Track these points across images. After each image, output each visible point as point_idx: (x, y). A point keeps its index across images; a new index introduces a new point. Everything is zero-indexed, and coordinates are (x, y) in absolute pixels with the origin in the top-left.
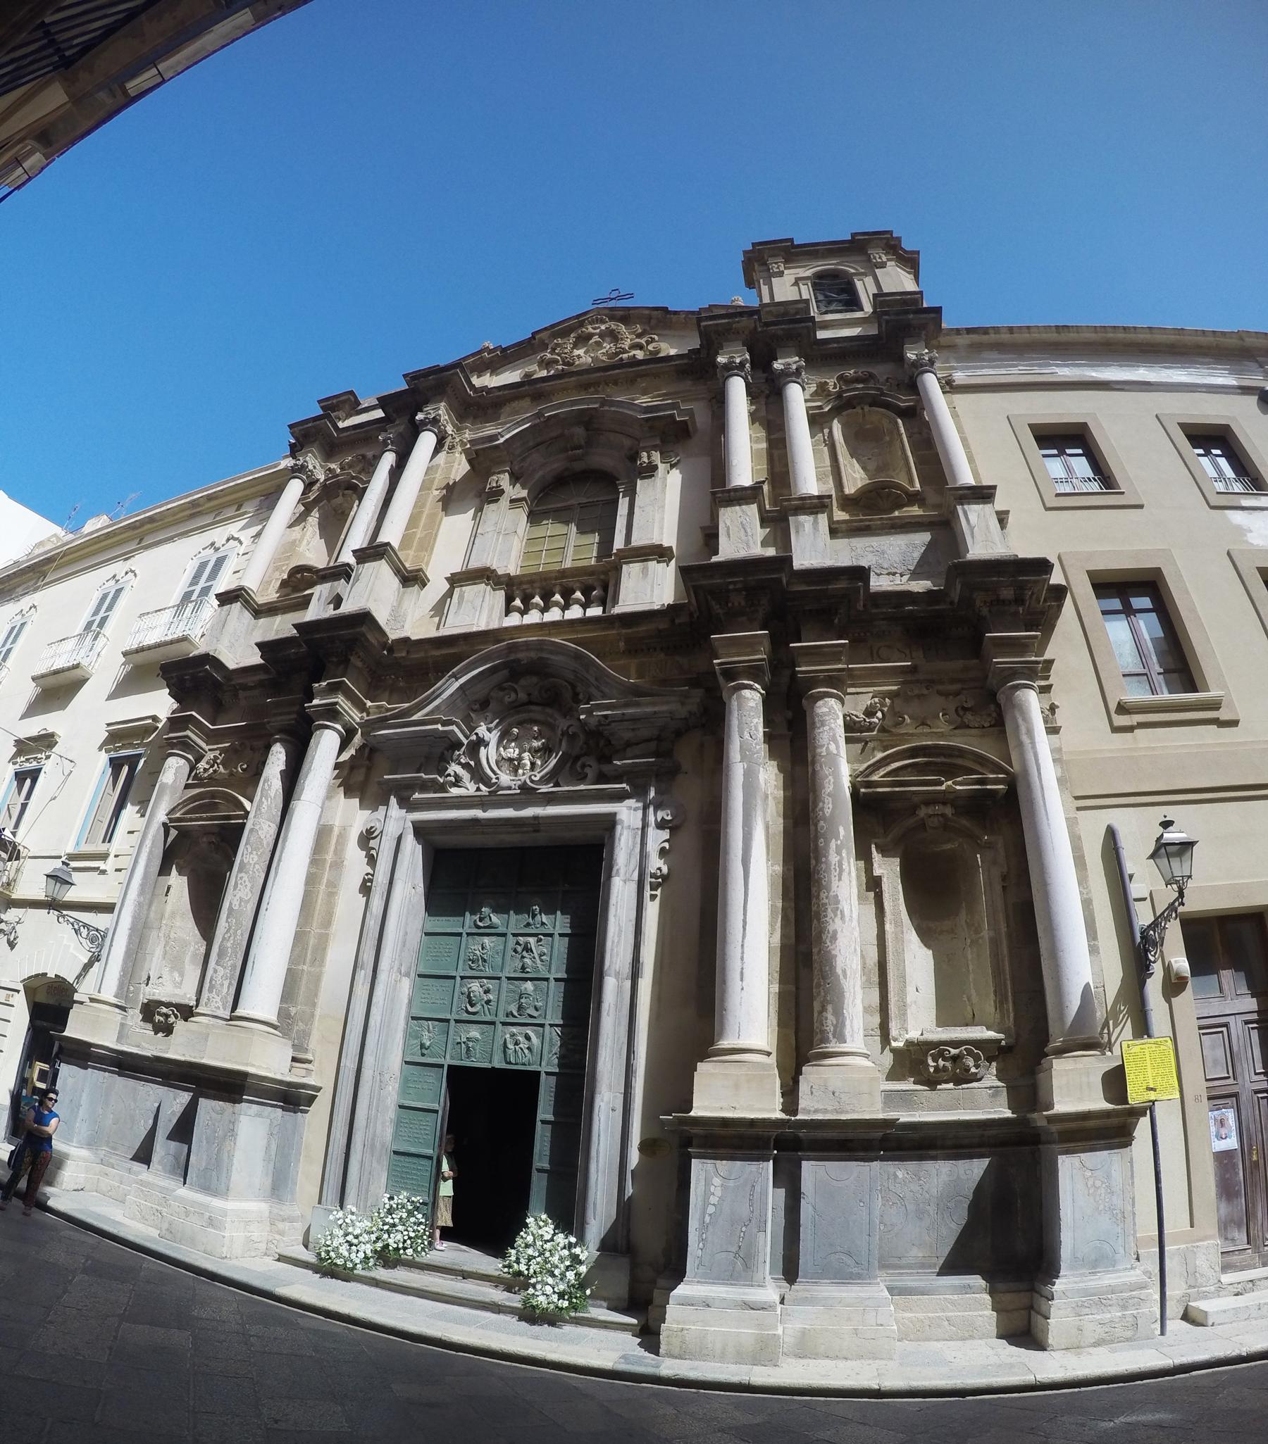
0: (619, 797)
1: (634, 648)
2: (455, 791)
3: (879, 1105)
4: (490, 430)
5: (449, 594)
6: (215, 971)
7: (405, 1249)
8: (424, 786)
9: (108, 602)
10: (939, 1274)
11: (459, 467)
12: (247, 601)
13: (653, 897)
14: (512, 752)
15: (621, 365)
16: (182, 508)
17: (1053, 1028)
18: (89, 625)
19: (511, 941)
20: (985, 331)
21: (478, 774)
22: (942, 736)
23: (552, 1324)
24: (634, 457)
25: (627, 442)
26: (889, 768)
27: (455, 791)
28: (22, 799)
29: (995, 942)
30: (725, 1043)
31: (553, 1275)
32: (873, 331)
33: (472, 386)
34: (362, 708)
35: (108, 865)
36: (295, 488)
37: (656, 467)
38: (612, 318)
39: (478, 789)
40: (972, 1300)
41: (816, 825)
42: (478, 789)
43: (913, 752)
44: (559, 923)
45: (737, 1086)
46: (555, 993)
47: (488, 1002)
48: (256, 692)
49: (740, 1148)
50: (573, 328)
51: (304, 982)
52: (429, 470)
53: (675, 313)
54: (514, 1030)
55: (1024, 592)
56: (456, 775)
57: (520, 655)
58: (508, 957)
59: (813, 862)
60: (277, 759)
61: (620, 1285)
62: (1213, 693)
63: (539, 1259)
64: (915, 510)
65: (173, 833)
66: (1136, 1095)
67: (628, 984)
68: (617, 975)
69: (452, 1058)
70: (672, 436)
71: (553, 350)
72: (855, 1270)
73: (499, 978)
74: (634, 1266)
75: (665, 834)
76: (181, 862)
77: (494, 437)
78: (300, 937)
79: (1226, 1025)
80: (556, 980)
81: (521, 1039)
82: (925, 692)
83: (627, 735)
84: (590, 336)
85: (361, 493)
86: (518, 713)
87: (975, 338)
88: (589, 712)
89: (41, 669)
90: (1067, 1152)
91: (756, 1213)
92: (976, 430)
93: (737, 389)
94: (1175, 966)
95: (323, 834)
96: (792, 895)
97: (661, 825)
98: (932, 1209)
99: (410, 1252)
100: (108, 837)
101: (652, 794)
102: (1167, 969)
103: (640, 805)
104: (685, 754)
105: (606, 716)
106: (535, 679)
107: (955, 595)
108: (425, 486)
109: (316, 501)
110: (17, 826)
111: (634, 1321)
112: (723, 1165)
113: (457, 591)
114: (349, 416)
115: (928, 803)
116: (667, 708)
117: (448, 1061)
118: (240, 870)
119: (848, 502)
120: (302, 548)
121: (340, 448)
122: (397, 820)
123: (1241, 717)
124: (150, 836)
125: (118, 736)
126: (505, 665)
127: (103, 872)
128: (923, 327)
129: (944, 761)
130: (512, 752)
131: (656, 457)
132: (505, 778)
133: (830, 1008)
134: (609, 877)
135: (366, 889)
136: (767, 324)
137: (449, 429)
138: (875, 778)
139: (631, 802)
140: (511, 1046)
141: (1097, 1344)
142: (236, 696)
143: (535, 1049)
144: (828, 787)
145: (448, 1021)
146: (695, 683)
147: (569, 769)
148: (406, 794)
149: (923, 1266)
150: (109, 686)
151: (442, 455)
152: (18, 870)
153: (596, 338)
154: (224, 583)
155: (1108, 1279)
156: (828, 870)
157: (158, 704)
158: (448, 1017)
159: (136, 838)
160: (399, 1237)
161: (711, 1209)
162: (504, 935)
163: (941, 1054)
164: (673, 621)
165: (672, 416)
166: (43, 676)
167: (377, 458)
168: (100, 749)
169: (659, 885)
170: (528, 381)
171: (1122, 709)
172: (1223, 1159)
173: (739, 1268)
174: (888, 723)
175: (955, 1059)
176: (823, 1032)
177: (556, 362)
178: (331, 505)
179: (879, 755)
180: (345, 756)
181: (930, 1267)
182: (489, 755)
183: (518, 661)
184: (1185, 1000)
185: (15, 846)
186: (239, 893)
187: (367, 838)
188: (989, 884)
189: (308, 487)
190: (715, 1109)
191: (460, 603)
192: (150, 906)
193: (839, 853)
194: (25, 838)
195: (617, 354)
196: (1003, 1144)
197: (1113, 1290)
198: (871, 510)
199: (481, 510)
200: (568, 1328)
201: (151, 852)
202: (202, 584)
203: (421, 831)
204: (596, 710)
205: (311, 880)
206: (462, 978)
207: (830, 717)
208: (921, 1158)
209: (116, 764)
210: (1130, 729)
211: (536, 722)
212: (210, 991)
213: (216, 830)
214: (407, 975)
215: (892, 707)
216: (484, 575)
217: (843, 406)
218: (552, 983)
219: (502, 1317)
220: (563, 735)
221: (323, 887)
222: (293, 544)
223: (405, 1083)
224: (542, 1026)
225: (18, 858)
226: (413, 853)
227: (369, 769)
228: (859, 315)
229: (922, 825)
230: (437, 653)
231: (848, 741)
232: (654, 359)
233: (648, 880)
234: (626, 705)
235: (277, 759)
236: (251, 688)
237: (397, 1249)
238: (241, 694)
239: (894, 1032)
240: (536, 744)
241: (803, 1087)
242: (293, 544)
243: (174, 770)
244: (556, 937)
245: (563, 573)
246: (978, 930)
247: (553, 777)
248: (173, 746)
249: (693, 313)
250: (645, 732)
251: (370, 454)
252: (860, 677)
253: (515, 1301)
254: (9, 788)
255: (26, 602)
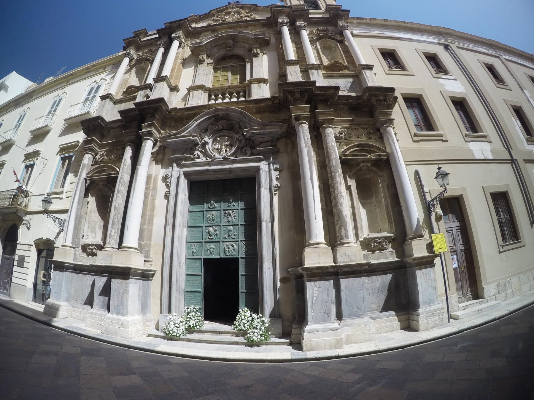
0: (260, 160)
1: (259, 111)
2: (198, 160)
3: (363, 259)
4: (197, 41)
5: (189, 94)
6: (111, 231)
7: (196, 326)
8: (186, 159)
9: (56, 104)
10: (381, 312)
11: (187, 52)
12: (111, 99)
13: (275, 194)
14: (218, 146)
15: (242, 21)
16: (83, 70)
17: (408, 231)
18: (50, 112)
19: (223, 212)
20: (362, 19)
21: (206, 154)
22: (363, 141)
23: (258, 346)
24: (250, 50)
25: (247, 46)
26: (351, 151)
27: (198, 160)
28: (28, 175)
29: (387, 206)
30: (312, 241)
31: (257, 329)
32: (327, 16)
33: (191, 27)
34: (160, 133)
35: (64, 196)
36: (126, 60)
37: (259, 54)
38: (237, 7)
39: (207, 159)
40: (391, 319)
41: (330, 169)
42: (207, 159)
43: (358, 146)
44: (240, 205)
45: (319, 256)
46: (241, 231)
47: (216, 234)
48: (117, 130)
49: (322, 276)
50: (224, 9)
51: (145, 233)
52: (177, 54)
53: (260, 6)
54: (227, 243)
55: (386, 96)
56: (198, 155)
57: (220, 113)
58: (222, 218)
59: (330, 181)
60: (129, 152)
61: (279, 329)
62: (440, 132)
63: (248, 324)
64: (346, 71)
65: (88, 182)
66: (436, 251)
67: (270, 224)
68: (266, 221)
69: (205, 255)
70: (264, 44)
71: (217, 17)
72: (360, 313)
73: (220, 226)
74: (283, 321)
75: (277, 173)
76: (92, 192)
77: (201, 43)
78: (143, 216)
79: (452, 230)
80: (241, 225)
81: (230, 247)
82: (358, 127)
83: (260, 140)
84: (230, 12)
85: (152, 62)
86: (219, 133)
87: (359, 21)
88: (248, 132)
89: (32, 128)
90: (418, 269)
91: (330, 298)
92: (364, 49)
93: (286, 30)
94: (439, 212)
95: (149, 177)
96: (323, 192)
97: (276, 170)
98: (377, 291)
99: (198, 327)
100: (63, 186)
101: (271, 159)
102: (436, 213)
103: (267, 163)
104: (281, 145)
105: (253, 133)
106: (225, 121)
107: (365, 98)
108: (176, 59)
109: (134, 65)
110: (27, 185)
111: (288, 341)
112: (317, 283)
113: (191, 93)
114: (144, 37)
115: (363, 162)
116: (275, 130)
117: (203, 257)
118: (118, 193)
119: (326, 68)
120: (130, 80)
121: (143, 47)
122: (177, 171)
123: (449, 139)
124: (80, 183)
125: (63, 149)
126: (214, 116)
127: (62, 198)
128: (344, 16)
129: (365, 149)
130: (218, 146)
131: (258, 50)
132: (217, 156)
133: (343, 228)
134: (259, 187)
135: (167, 196)
136: (293, 11)
137: (183, 40)
138: (347, 153)
139: (264, 162)
140: (227, 249)
141: (432, 328)
142: (109, 132)
143: (236, 249)
144: (333, 156)
145: (202, 242)
146: (283, 122)
147: (240, 151)
148: (179, 162)
149: (376, 310)
150: (59, 132)
151: (181, 49)
152: (29, 201)
153: (232, 13)
154: (101, 92)
155: (433, 308)
156: (337, 183)
157: (80, 136)
158: (202, 241)
159: (74, 185)
160: (194, 322)
161: (315, 299)
162: (220, 210)
163: (376, 242)
164: (273, 102)
165: (263, 38)
166: (34, 131)
167: (157, 50)
168: (57, 154)
169: (277, 190)
170: (209, 26)
171: (415, 135)
172: (455, 269)
173: (325, 319)
174: (347, 137)
175: (380, 243)
176: (341, 236)
177: (219, 20)
178: (141, 66)
179: (345, 148)
180: (155, 150)
181: (378, 310)
182: (209, 147)
183: (218, 115)
184: (442, 222)
185: (27, 191)
186: (118, 201)
187: (165, 179)
188: (383, 187)
189: (131, 60)
190: (312, 264)
191: (193, 97)
192: (82, 209)
193: (339, 177)
194: (31, 188)
195: (240, 18)
196: (396, 269)
197: (435, 310)
198: (333, 70)
199: (197, 67)
200: (264, 347)
201: (81, 189)
202: (92, 94)
203: (186, 175)
204: (249, 131)
205: (146, 195)
206: (206, 227)
207: (331, 133)
208: (372, 275)
209: (63, 159)
210: (418, 141)
211: (226, 136)
212: (110, 238)
213: (105, 179)
214: (185, 227)
215: (347, 132)
216: (201, 87)
217: (320, 38)
218: (240, 226)
219: (239, 346)
220: (237, 139)
221: (150, 197)
222: (127, 80)
223: (188, 267)
224: (238, 241)
225: (28, 196)
226: (184, 183)
227: (164, 154)
228: (320, 11)
229: (361, 169)
230: (187, 113)
231: (337, 142)
232: (254, 20)
233: (273, 188)
234: (261, 129)
235: (129, 152)
236: (116, 128)
237: (193, 327)
238: (111, 131)
239: (360, 236)
240: (227, 143)
241: (338, 255)
242: (127, 80)
243: (87, 159)
244: (240, 210)
245: (229, 87)
246: (380, 202)
247: (234, 154)
248: (86, 150)
249: (265, 7)
250: (267, 139)
251: (153, 49)
252: (336, 122)
253: (242, 339)
254: (23, 172)
255: (25, 107)
